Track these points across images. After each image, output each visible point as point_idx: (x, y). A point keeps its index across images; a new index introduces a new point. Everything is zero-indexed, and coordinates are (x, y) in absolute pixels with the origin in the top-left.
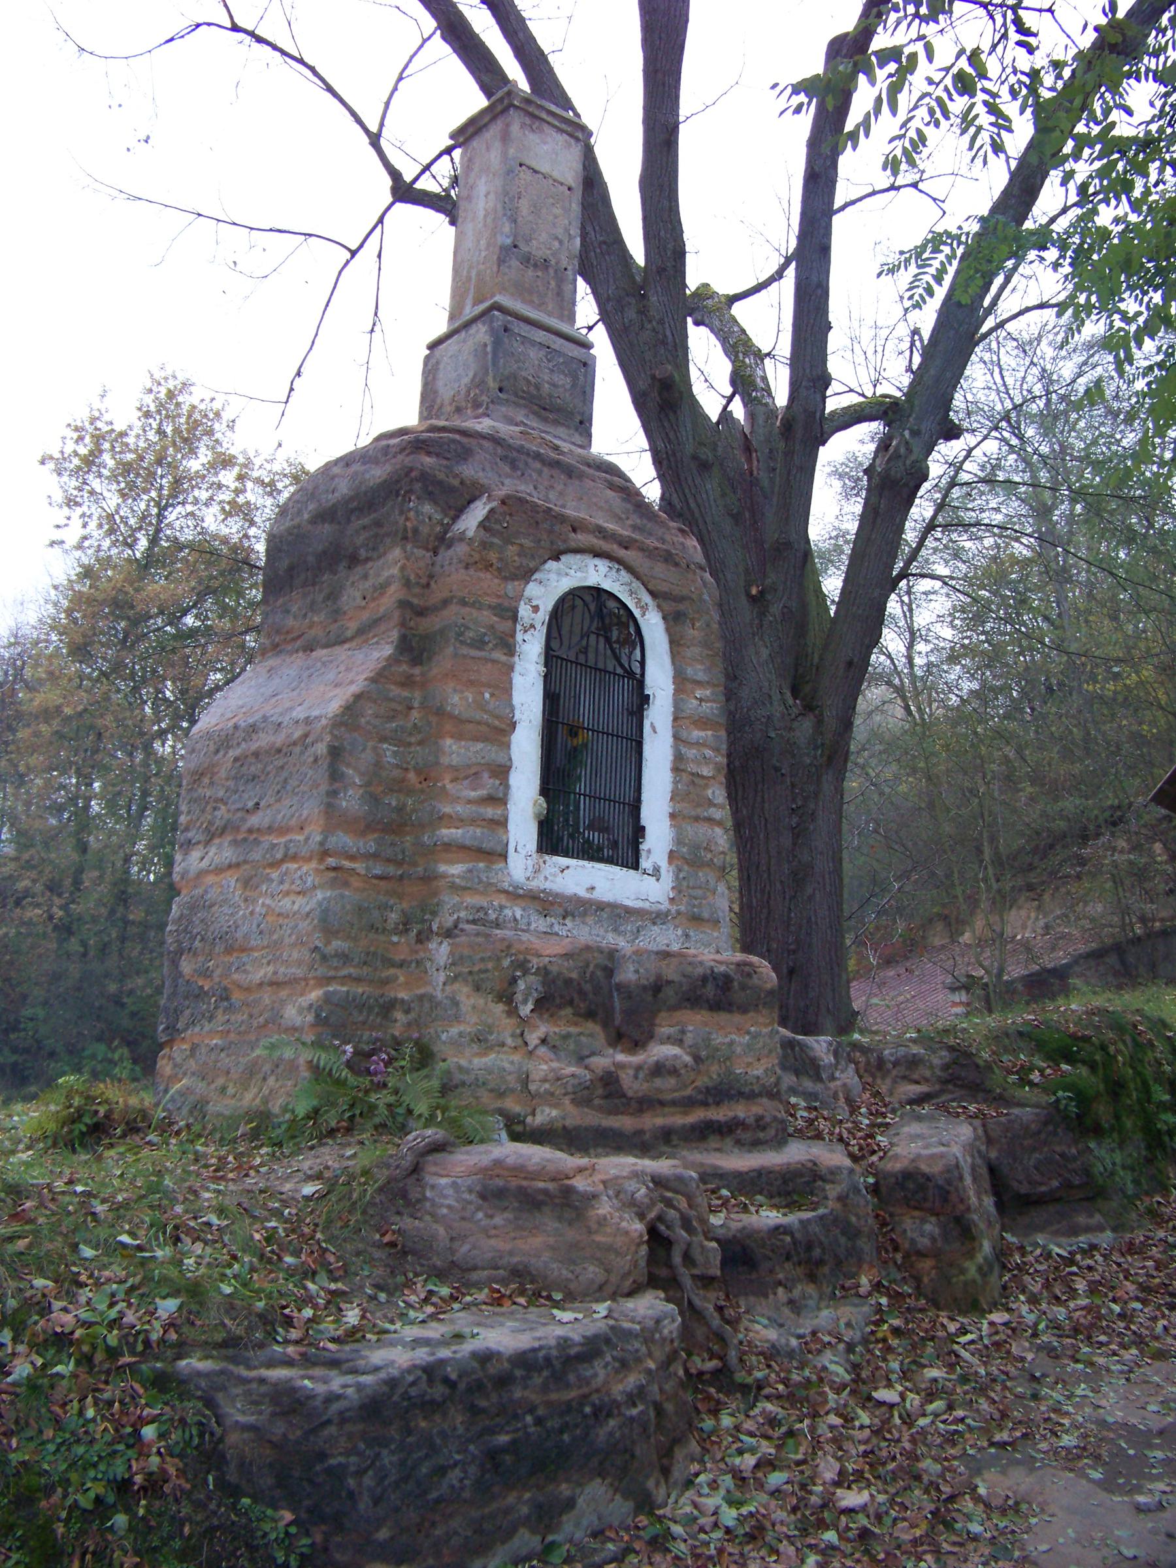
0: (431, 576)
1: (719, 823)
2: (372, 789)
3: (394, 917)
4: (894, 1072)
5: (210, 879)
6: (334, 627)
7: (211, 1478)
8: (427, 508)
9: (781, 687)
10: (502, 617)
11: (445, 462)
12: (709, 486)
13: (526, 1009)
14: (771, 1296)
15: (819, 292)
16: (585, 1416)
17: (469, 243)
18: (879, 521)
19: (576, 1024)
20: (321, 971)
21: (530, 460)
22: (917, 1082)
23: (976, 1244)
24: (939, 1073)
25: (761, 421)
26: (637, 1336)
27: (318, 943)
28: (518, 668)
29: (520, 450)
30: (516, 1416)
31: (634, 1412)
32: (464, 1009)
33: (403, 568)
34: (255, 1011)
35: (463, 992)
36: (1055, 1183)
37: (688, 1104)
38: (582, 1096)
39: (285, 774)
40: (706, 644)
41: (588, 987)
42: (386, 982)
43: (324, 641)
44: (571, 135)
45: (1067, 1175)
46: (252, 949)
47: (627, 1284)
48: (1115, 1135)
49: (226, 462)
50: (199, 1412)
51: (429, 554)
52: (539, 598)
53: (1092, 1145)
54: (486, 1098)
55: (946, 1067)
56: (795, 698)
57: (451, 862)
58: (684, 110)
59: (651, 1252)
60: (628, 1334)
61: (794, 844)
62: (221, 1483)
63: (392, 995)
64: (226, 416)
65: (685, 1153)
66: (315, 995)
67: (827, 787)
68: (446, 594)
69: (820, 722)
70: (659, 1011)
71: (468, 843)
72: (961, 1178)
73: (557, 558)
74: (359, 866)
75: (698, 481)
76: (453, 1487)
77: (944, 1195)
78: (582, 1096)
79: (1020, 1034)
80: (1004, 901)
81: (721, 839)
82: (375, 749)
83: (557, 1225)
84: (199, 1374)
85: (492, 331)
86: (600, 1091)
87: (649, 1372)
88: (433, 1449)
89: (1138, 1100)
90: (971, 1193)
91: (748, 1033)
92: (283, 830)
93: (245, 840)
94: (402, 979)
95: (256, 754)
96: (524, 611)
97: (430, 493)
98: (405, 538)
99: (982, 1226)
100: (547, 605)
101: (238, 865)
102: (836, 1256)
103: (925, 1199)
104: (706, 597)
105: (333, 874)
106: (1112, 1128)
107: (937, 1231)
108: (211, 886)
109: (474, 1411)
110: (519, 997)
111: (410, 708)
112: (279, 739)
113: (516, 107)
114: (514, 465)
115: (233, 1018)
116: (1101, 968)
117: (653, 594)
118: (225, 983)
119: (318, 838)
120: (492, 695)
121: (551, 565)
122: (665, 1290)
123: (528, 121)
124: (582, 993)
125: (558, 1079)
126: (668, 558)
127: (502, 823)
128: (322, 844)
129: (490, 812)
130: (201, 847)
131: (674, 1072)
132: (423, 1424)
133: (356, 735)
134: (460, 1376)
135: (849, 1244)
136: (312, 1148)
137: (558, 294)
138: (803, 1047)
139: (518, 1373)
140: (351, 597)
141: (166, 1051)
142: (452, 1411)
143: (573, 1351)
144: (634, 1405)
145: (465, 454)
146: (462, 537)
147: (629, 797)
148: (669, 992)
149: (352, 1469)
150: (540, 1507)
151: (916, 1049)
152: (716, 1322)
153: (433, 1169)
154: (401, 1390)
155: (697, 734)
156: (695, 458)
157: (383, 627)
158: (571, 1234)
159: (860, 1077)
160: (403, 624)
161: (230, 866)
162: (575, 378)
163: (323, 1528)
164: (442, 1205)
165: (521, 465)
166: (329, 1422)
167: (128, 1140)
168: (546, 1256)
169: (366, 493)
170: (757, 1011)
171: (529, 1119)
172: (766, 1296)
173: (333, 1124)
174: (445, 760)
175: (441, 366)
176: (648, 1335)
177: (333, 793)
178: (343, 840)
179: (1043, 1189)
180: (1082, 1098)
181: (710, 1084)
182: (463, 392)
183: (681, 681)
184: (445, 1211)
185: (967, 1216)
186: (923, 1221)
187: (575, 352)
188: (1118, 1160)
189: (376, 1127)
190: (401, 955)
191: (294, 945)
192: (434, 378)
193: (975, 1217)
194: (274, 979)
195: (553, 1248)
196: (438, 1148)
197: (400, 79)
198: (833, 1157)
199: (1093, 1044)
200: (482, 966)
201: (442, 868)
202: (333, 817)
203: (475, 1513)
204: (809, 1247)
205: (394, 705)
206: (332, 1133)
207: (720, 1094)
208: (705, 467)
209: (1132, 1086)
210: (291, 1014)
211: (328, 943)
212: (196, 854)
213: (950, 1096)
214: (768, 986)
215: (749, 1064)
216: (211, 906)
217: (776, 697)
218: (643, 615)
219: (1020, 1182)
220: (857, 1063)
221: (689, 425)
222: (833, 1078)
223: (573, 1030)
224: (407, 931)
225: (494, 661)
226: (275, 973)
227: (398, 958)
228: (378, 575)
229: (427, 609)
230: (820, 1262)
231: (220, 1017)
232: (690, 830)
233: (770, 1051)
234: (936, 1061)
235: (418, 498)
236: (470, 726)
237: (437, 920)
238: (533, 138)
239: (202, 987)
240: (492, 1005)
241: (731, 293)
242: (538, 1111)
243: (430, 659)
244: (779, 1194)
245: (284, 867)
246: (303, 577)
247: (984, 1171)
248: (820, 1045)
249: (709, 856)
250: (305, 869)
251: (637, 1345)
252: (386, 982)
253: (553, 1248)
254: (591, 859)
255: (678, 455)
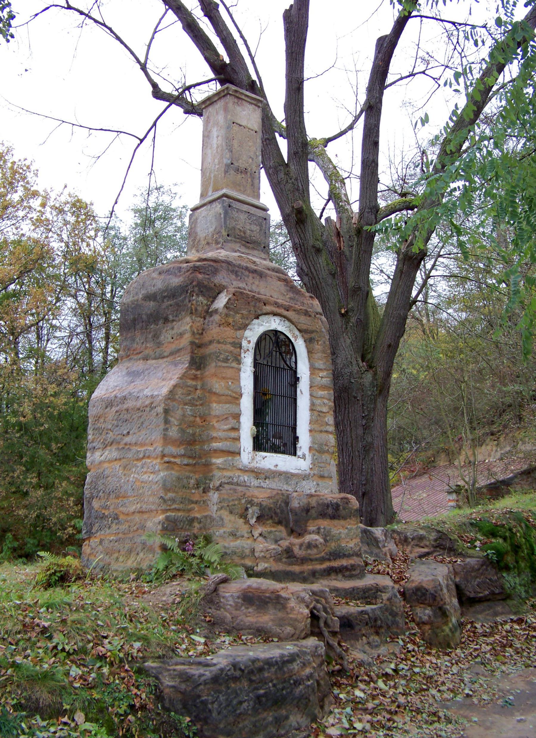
0: (203, 330)
1: (331, 433)
2: (181, 426)
3: (192, 481)
4: (412, 543)
5: (106, 465)
6: (158, 350)
7: (159, 705)
8: (201, 298)
9: (356, 358)
10: (235, 348)
11: (207, 276)
12: (320, 261)
13: (253, 521)
14: (360, 641)
15: (373, 165)
16: (291, 684)
17: (209, 159)
18: (403, 275)
19: (274, 527)
20: (164, 507)
21: (244, 271)
22: (423, 547)
23: (449, 619)
24: (433, 543)
25: (345, 221)
26: (308, 654)
27: (162, 495)
28: (242, 369)
29: (239, 266)
30: (266, 683)
31: (309, 683)
32: (225, 521)
33: (191, 327)
34: (132, 524)
35: (225, 514)
36: (487, 592)
37: (322, 560)
38: (277, 558)
39: (142, 420)
40: (324, 352)
41: (278, 511)
42: (189, 510)
43: (153, 356)
44: (256, 105)
45: (492, 589)
46: (129, 497)
47: (303, 635)
48: (516, 570)
49: (35, 194)
50: (154, 681)
51: (202, 319)
52: (250, 337)
53: (504, 575)
54: (237, 559)
55: (436, 540)
56: (363, 361)
57: (218, 458)
58: (306, 75)
59: (312, 621)
60: (305, 653)
61: (364, 433)
62: (163, 707)
63: (193, 515)
64: (32, 168)
65: (321, 581)
66: (161, 517)
67: (379, 405)
68: (210, 338)
69: (375, 374)
70: (309, 520)
71: (224, 449)
72: (441, 590)
73: (257, 318)
74: (178, 461)
75: (315, 258)
76: (244, 709)
77: (434, 597)
78: (277, 558)
79: (472, 524)
80: (478, 442)
81: (332, 439)
82: (182, 408)
83: (274, 611)
84: (152, 668)
85: (224, 207)
86: (285, 556)
87: (314, 668)
88: (237, 695)
89: (528, 554)
90: (446, 597)
91: (347, 528)
92: (142, 445)
93: (123, 448)
94: (196, 509)
95: (127, 410)
96: (244, 343)
97: (202, 292)
98: (191, 313)
99: (452, 611)
100: (254, 340)
101: (120, 459)
102: (387, 624)
103: (426, 599)
104: (323, 330)
105: (167, 465)
106: (514, 567)
107: (431, 613)
108: (107, 468)
109: (251, 681)
110: (249, 516)
111: (196, 389)
112: (139, 404)
113: (230, 94)
114: (236, 274)
115: (120, 527)
116: (530, 479)
117: (300, 331)
118: (116, 512)
119: (161, 449)
120: (232, 383)
121: (255, 321)
122: (317, 637)
123: (236, 100)
124: (275, 513)
125: (267, 551)
126: (306, 313)
127: (237, 439)
128: (162, 452)
129: (233, 434)
130: (100, 450)
131: (316, 546)
132: (233, 685)
133: (174, 403)
134: (245, 668)
135: (393, 619)
136: (167, 583)
137: (252, 185)
138: (370, 532)
139: (266, 667)
140: (166, 336)
141: (87, 542)
142: (243, 681)
143: (286, 659)
144: (309, 681)
145: (215, 272)
146: (216, 311)
147: (291, 423)
148: (313, 512)
149: (210, 701)
150: (276, 718)
151: (422, 532)
152: (339, 650)
153: (223, 590)
154: (225, 673)
155: (321, 393)
156: (314, 247)
157: (182, 353)
158: (280, 614)
159: (397, 545)
160: (192, 352)
161: (116, 460)
162: (261, 226)
163: (201, 723)
164: (227, 605)
165: (240, 274)
166: (201, 684)
167: (77, 583)
168: (270, 624)
169: (171, 290)
170: (350, 519)
171: (255, 568)
172: (358, 640)
173: (175, 573)
174: (213, 413)
175: (199, 221)
176: (314, 654)
177: (166, 430)
178: (172, 449)
179: (481, 595)
180: (500, 554)
181: (332, 551)
182: (210, 235)
183: (313, 369)
184: (229, 607)
185: (445, 606)
186: (425, 609)
187: (260, 213)
188: (517, 582)
189: (193, 573)
190: (196, 498)
191: (151, 495)
192: (195, 227)
193: (448, 607)
194: (141, 510)
195: (272, 620)
196: (224, 581)
197: (155, 32)
198: (386, 581)
199: (505, 528)
200: (233, 503)
201: (214, 460)
202: (166, 439)
203: (253, 719)
204: (376, 620)
205: (189, 389)
206: (174, 576)
207: (336, 555)
208: (318, 251)
209: (524, 547)
210: (149, 524)
211: (166, 495)
212: (98, 454)
213: (438, 553)
214: (355, 508)
215: (348, 542)
216: (107, 477)
217: (354, 363)
218: (296, 340)
219: (470, 592)
220: (395, 539)
221: (310, 230)
222: (384, 546)
223: (273, 529)
224: (198, 488)
225: (232, 368)
226: (141, 507)
227: (195, 499)
228: (179, 329)
229: (202, 344)
230: (381, 627)
231: (114, 526)
232: (318, 436)
233: (357, 536)
234: (431, 538)
235: (197, 295)
236: (223, 397)
237: (212, 483)
238: (239, 109)
239: (104, 514)
240: (238, 520)
241: (327, 137)
242: (259, 565)
243: (204, 368)
244: (362, 598)
245: (144, 461)
246: (141, 324)
247: (453, 587)
248: (378, 532)
249: (327, 448)
250: (154, 462)
251: (309, 657)
252: (189, 510)
253: (272, 620)
254: (276, 452)
255: (306, 245)
